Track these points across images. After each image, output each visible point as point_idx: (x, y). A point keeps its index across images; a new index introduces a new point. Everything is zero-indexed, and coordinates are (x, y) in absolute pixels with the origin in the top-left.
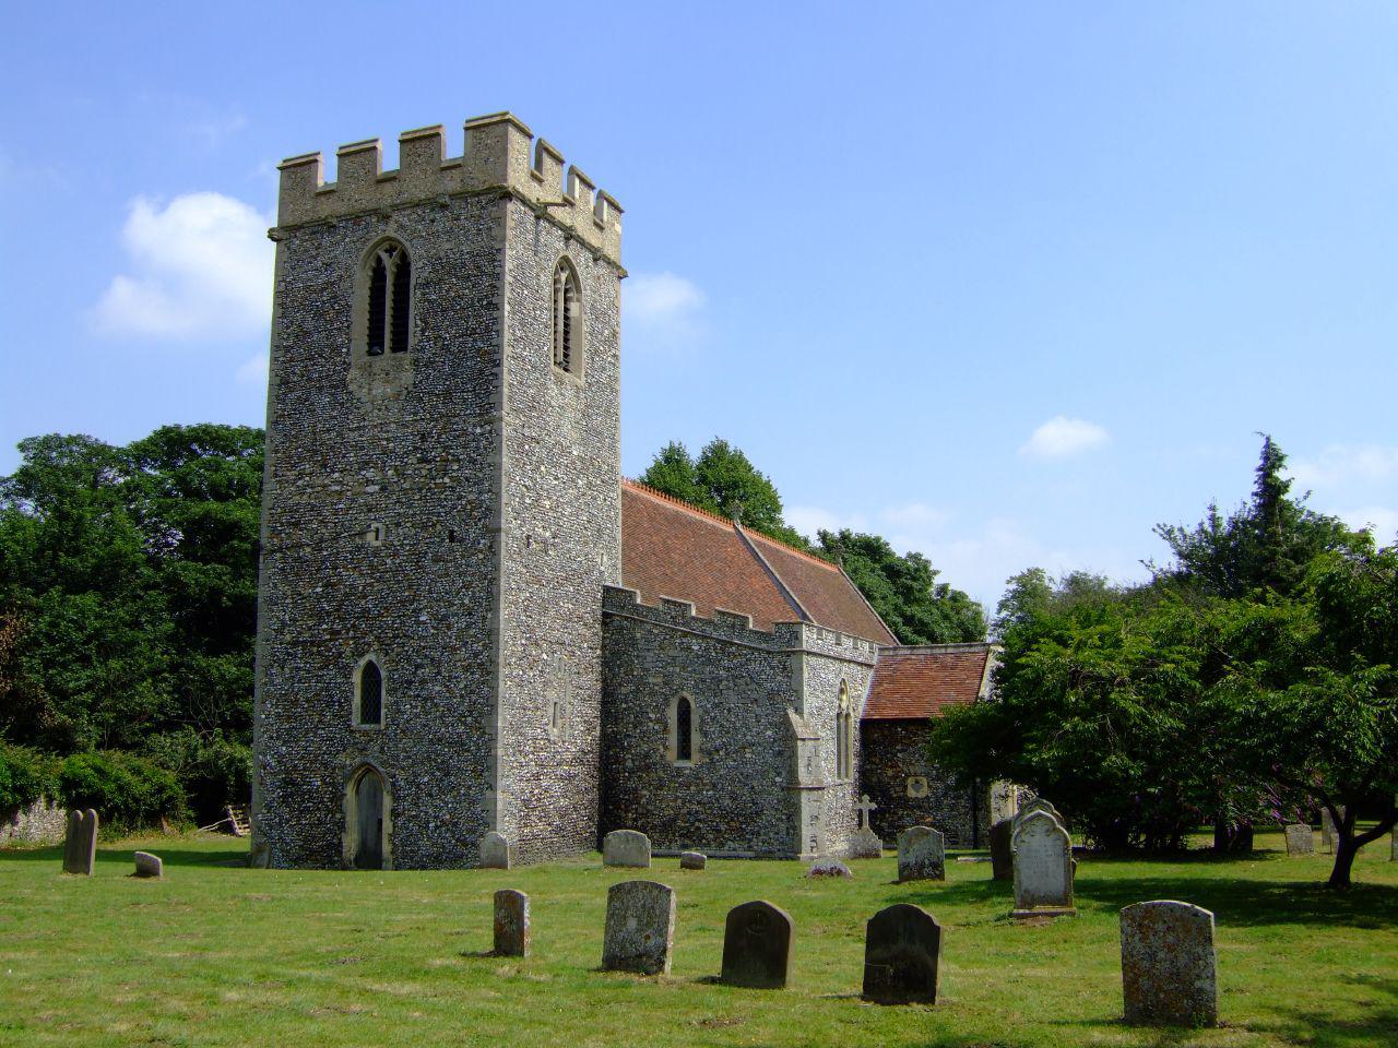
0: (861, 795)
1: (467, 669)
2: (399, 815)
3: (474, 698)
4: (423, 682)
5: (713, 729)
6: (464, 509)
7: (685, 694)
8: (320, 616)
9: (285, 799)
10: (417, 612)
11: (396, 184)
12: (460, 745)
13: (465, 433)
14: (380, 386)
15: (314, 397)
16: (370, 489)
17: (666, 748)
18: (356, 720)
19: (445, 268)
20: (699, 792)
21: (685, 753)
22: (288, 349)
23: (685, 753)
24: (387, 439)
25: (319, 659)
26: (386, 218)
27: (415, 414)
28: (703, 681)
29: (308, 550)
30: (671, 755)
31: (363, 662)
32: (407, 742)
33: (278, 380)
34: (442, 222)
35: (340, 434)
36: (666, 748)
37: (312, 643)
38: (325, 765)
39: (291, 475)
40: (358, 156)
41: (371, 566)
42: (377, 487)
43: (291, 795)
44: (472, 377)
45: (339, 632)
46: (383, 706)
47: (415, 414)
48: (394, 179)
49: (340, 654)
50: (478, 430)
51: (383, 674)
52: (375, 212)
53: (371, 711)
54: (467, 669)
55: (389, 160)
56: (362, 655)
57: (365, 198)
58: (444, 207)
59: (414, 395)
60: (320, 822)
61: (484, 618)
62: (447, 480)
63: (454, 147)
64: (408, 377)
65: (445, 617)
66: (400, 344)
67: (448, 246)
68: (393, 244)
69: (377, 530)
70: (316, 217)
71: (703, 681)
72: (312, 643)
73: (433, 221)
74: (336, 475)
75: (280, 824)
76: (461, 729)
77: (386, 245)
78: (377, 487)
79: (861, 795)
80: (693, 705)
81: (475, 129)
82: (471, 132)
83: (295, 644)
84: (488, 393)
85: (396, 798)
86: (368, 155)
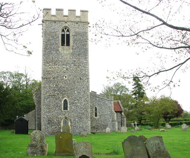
0: (28, 134)
1: (84, 101)
2: (72, 126)
3: (86, 106)
4: (76, 103)
5: (100, 112)
6: (82, 74)
7: (96, 106)
8: (55, 91)
9: (49, 123)
10: (74, 91)
11: (67, 17)
12: (83, 114)
13: (82, 62)
14: (65, 52)
15: (52, 52)
16: (64, 69)
17: (93, 115)
18: (63, 110)
19: (77, 34)
20: (99, 122)
21: (96, 115)
22: (46, 42)
23: (96, 115)
24: (68, 61)
25: (55, 98)
26: (66, 23)
27: (73, 57)
28: (99, 104)
29: (52, 79)
30: (94, 116)
31: (64, 99)
32: (73, 113)
33: (44, 47)
34: (76, 25)
35: (58, 59)
36: (93, 115)
37: (53, 95)
38: (57, 117)
39: (48, 65)
40: (72, 11)
41: (65, 82)
42: (66, 69)
43: (50, 123)
44: (83, 51)
45: (59, 94)
46: (68, 107)
47: (73, 57)
48: (67, 16)
49: (59, 98)
50: (85, 61)
51: (68, 101)
52: (64, 21)
53: (66, 108)
54: (84, 101)
55: (53, 12)
56: (64, 98)
57: (60, 18)
58: (77, 23)
59: (73, 54)
60: (56, 127)
61: (87, 93)
62: (79, 69)
63: (78, 13)
64: (71, 51)
65: (80, 92)
66: (68, 44)
67: (78, 30)
68: (66, 27)
69: (66, 76)
70: (51, 20)
71: (99, 104)
72: (53, 95)
73: (75, 25)
74: (57, 66)
75: (48, 128)
76: (83, 111)
77: (65, 27)
78: (66, 69)
79: (28, 134)
80: (97, 108)
81: (82, 11)
82: (81, 12)
83: (50, 95)
84: (86, 55)
85: (71, 123)
86: (62, 11)
